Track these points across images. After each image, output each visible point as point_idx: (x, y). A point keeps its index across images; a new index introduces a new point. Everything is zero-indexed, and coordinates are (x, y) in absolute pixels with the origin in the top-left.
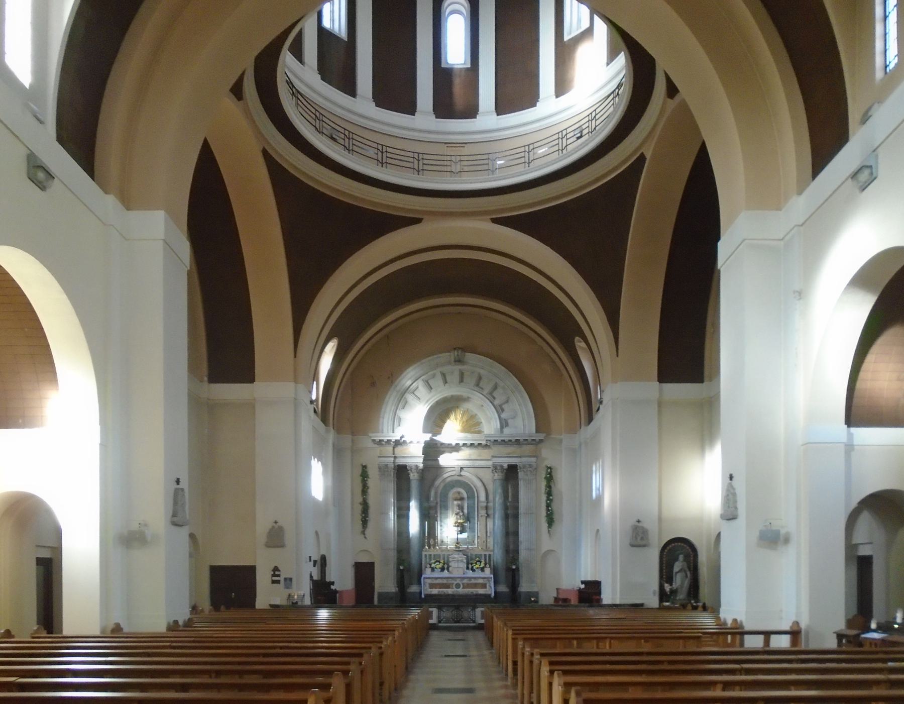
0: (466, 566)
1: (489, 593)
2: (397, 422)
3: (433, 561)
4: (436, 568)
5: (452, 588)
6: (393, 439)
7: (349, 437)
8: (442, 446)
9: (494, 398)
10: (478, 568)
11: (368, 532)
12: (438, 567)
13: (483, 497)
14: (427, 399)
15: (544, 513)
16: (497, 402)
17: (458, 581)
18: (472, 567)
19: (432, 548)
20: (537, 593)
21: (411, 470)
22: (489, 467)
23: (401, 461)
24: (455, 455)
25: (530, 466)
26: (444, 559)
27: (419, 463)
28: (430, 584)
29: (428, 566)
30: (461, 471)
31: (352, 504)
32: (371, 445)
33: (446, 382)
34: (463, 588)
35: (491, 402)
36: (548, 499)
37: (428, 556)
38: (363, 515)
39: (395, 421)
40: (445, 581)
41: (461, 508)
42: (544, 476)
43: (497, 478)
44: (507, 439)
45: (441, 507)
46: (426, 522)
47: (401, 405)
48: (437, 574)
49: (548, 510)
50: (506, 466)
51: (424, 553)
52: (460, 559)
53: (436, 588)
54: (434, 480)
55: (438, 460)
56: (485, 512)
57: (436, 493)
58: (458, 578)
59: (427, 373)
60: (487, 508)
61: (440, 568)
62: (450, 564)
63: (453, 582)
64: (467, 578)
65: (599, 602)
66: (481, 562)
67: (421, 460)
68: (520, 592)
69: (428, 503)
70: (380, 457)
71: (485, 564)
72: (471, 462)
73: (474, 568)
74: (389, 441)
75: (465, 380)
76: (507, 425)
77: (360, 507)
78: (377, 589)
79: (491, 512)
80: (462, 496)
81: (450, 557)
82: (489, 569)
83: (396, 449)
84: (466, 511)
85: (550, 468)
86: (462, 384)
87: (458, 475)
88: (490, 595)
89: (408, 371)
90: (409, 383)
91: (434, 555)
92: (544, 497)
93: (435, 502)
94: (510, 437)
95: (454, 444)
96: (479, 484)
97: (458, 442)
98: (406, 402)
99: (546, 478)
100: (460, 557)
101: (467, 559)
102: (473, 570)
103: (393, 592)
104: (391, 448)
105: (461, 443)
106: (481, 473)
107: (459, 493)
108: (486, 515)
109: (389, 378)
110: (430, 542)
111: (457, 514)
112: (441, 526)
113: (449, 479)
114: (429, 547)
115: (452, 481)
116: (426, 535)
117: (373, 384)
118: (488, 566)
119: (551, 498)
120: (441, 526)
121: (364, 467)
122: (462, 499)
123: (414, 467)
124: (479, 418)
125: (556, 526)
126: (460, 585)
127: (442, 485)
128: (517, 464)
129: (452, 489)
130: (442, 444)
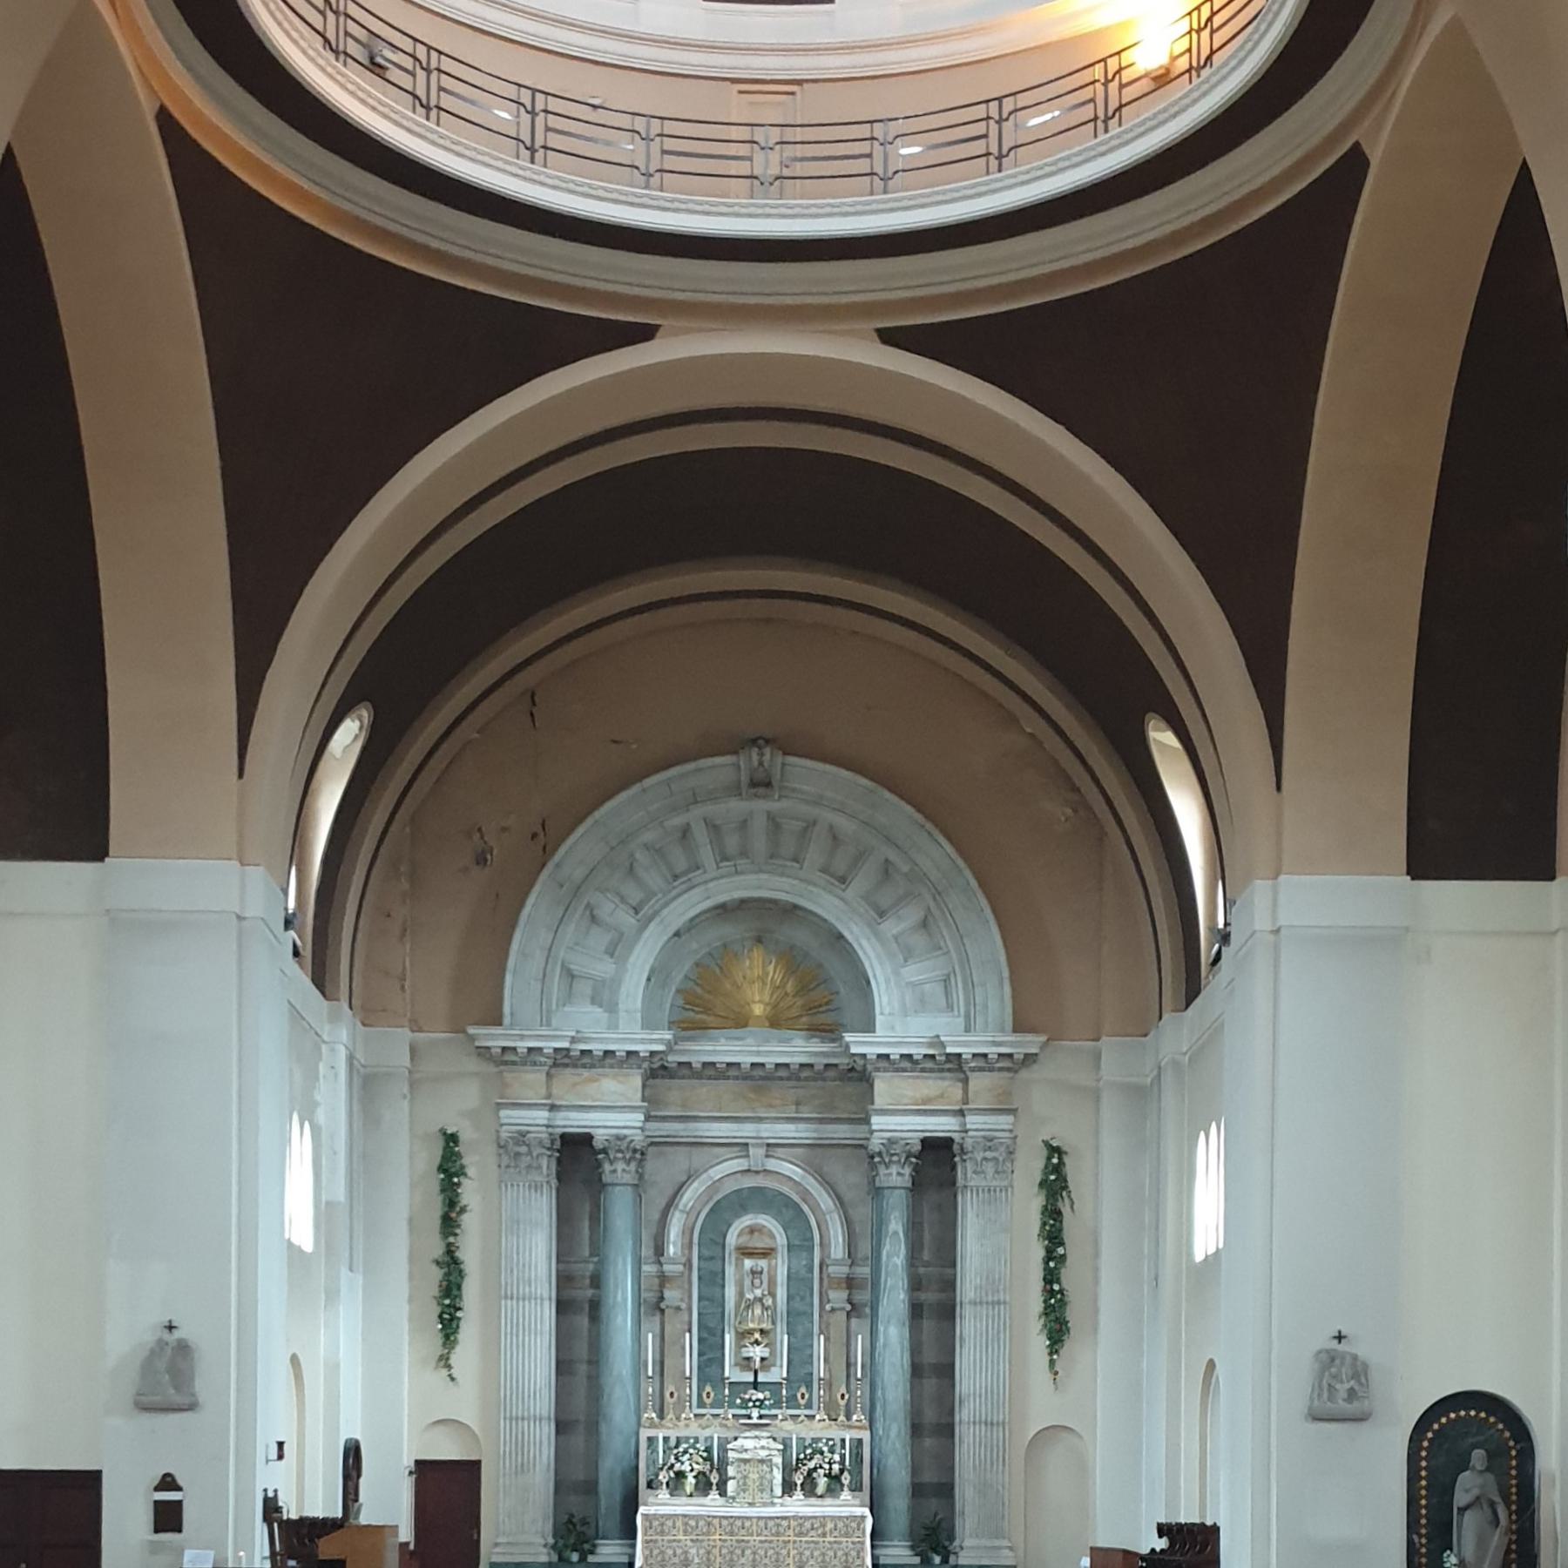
49: (1051, 1293)
51: (645, 1433)
52: (763, 1454)
81: (729, 1446)
100: (763, 1448)
108: (849, 1307)
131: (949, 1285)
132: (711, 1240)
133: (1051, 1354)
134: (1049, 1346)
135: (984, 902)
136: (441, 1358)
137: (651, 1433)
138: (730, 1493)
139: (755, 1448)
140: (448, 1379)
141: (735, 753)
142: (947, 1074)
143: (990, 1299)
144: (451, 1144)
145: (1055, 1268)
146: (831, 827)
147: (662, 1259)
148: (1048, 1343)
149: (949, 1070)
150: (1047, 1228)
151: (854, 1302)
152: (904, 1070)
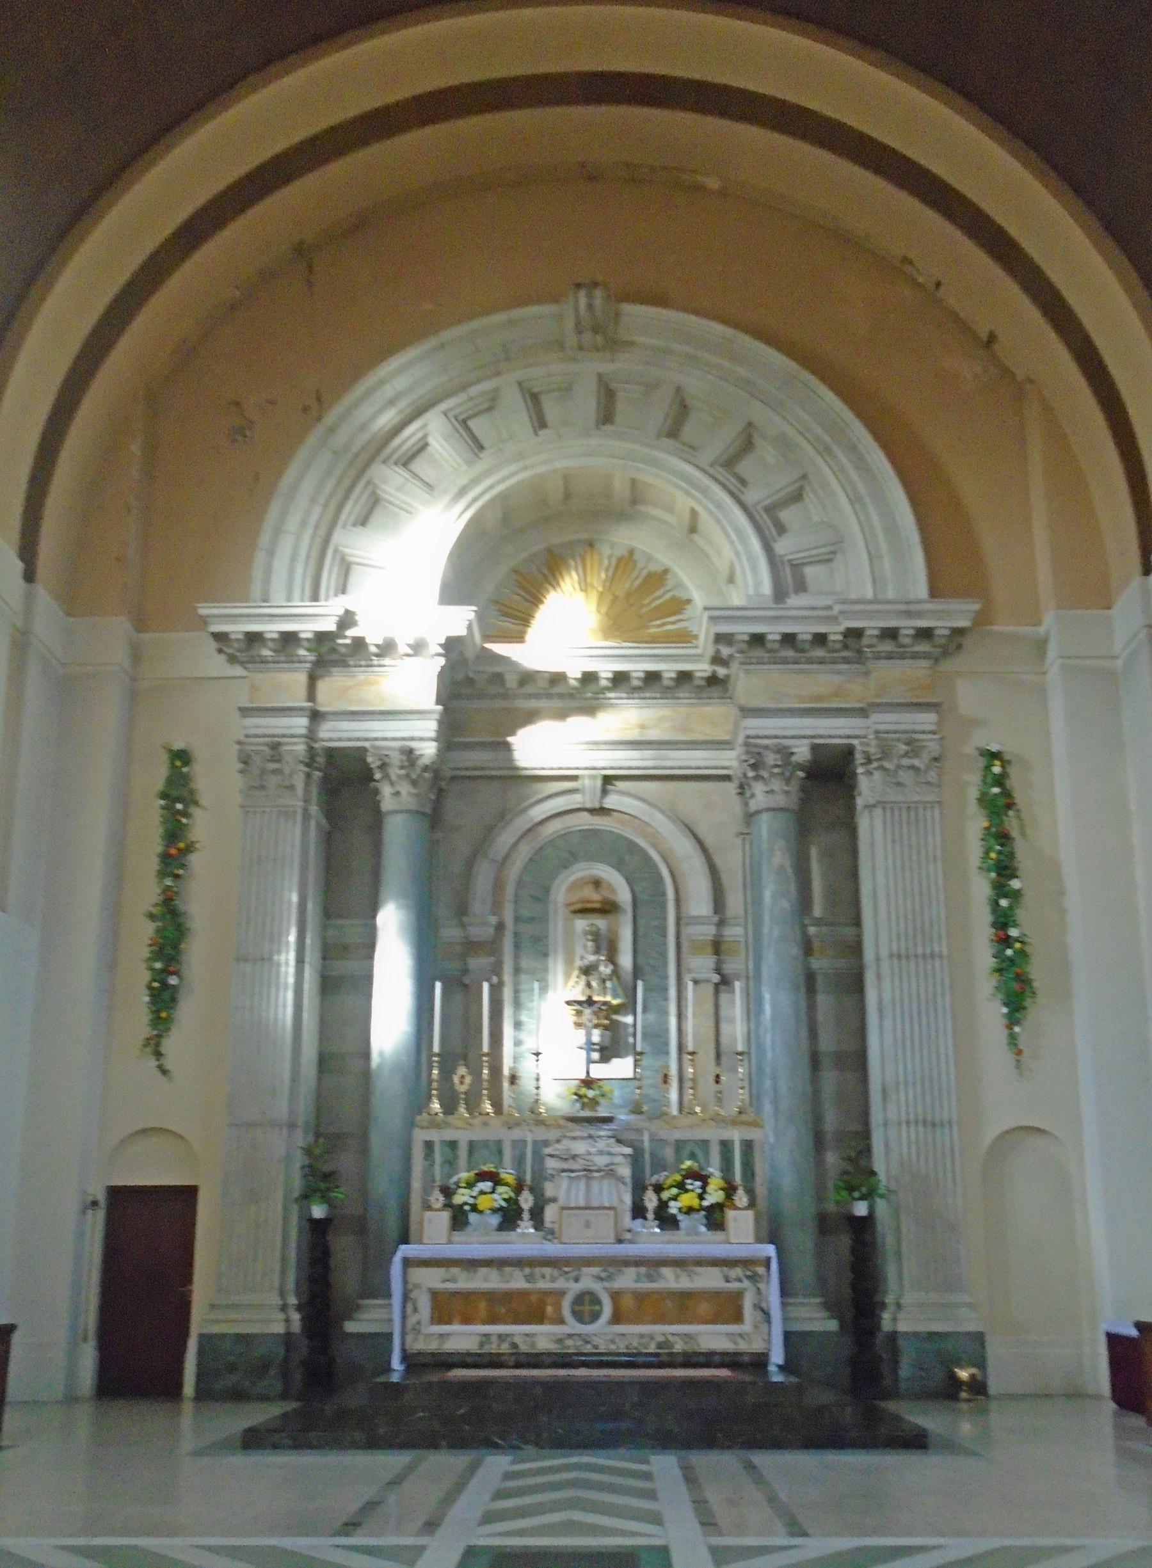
0: (628, 1199)
1: (757, 1346)
2: (335, 571)
3: (464, 1175)
4: (474, 1208)
5: (561, 1321)
6: (306, 629)
7: (118, 626)
8: (529, 689)
9: (743, 482)
10: (690, 1210)
11: (170, 1045)
12: (484, 1202)
13: (700, 904)
14: (463, 481)
15: (984, 956)
16: (754, 495)
17: (588, 1281)
18: (663, 1205)
19: (462, 1109)
20: (979, 1338)
21: (383, 766)
22: (727, 778)
23: (337, 733)
24: (579, 726)
25: (914, 747)
26: (519, 1162)
27: (422, 739)
28: (436, 1296)
29: (438, 1199)
30: (605, 792)
31: (114, 912)
32: (217, 665)
33: (540, 423)
34: (616, 1319)
35: (732, 494)
36: (1000, 889)
37: (437, 1148)
38: (158, 965)
39: (325, 574)
40: (517, 1282)
41: (607, 946)
42: (973, 793)
43: (762, 806)
44: (805, 630)
45: (517, 946)
46: (438, 986)
47: (351, 509)
48: (470, 1245)
49: (1005, 941)
50: (802, 752)
51: (420, 1136)
52: (602, 1161)
53: (467, 1321)
54: (489, 833)
55: (507, 747)
56: (709, 962)
57: (498, 886)
58: (588, 1262)
59: (464, 388)
60: (717, 947)
61: (495, 1211)
62: (549, 1189)
63: (560, 1284)
64: (638, 1262)
65: (310, 1166)
66: (704, 1179)
67: (429, 727)
68: (893, 1336)
69: (463, 925)
70: (245, 712)
71: (730, 1190)
72: (648, 753)
73: (673, 1208)
74: (289, 639)
75: (619, 418)
76: (801, 586)
77: (149, 929)
78: (201, 1321)
79: (732, 966)
80: (612, 897)
81: (548, 1151)
82: (750, 1214)
83: (322, 686)
84: (626, 960)
85: (995, 756)
86: (609, 428)
87: (592, 811)
88: (760, 1362)
89: (386, 369)
90: (388, 418)
91: (472, 1146)
92: (981, 887)
93: (493, 920)
94: (818, 620)
95: (574, 673)
96: (683, 847)
97: (591, 667)
98: (375, 502)
99: (984, 800)
100: (601, 1153)
101: (636, 1160)
102: (667, 1221)
103: (278, 1335)
104: (301, 678)
105: (606, 669)
106: (689, 794)
107: (597, 883)
108: (716, 978)
109: (306, 409)
110: (456, 1079)
111: (587, 971)
112: (518, 1025)
113: (555, 826)
114: (449, 1108)
115: (565, 836)
116: (436, 1048)
117: (239, 432)
118: (741, 1198)
119: (1015, 884)
120: (518, 1025)
121: (182, 757)
122: (608, 908)
123: (396, 758)
124: (680, 585)
125: (1038, 1011)
126: (596, 1301)
127: (525, 851)
128: (855, 742)
129: (565, 866)
130: (528, 677)
131: (856, 949)
132: (532, 896)
133: (1010, 1026)
134: (1005, 1015)
135: (878, 459)
136: (147, 1042)
137: (434, 1136)
138: (548, 1224)
139: (589, 1154)
140: (158, 1074)
141: (556, 300)
142: (843, 667)
143: (920, 951)
144: (178, 763)
145: (1010, 908)
146: (678, 389)
147: (465, 919)
148: (1005, 1010)
149: (846, 661)
150: (993, 855)
151: (725, 972)
152: (785, 661)
